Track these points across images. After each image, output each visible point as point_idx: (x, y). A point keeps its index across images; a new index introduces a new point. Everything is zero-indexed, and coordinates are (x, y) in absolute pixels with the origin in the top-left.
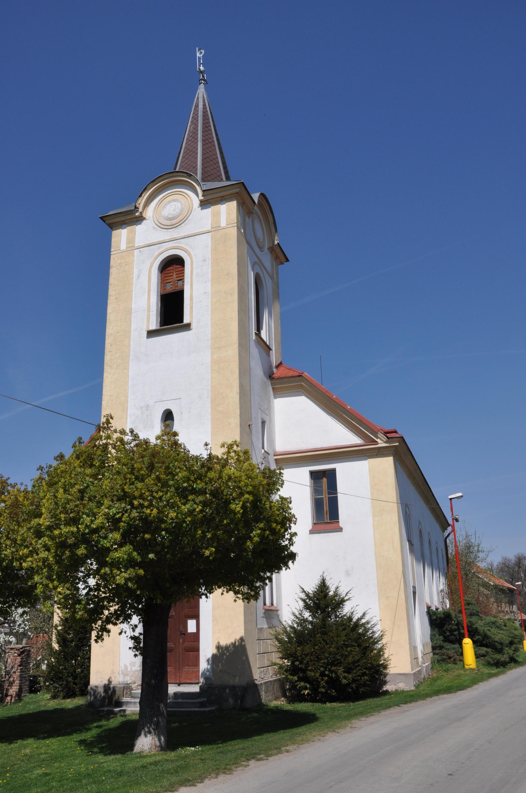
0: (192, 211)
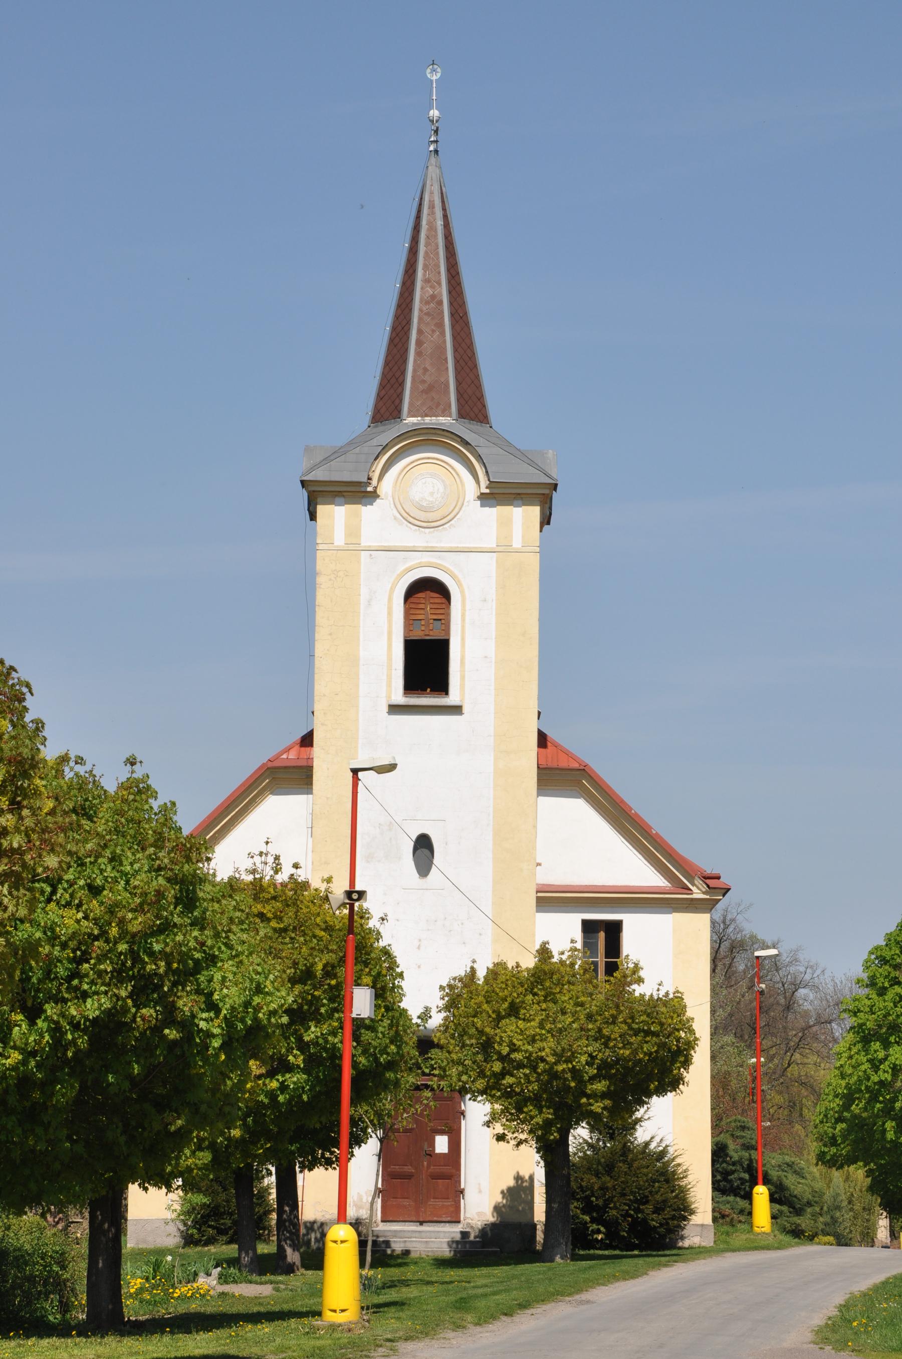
0: (463, 504)
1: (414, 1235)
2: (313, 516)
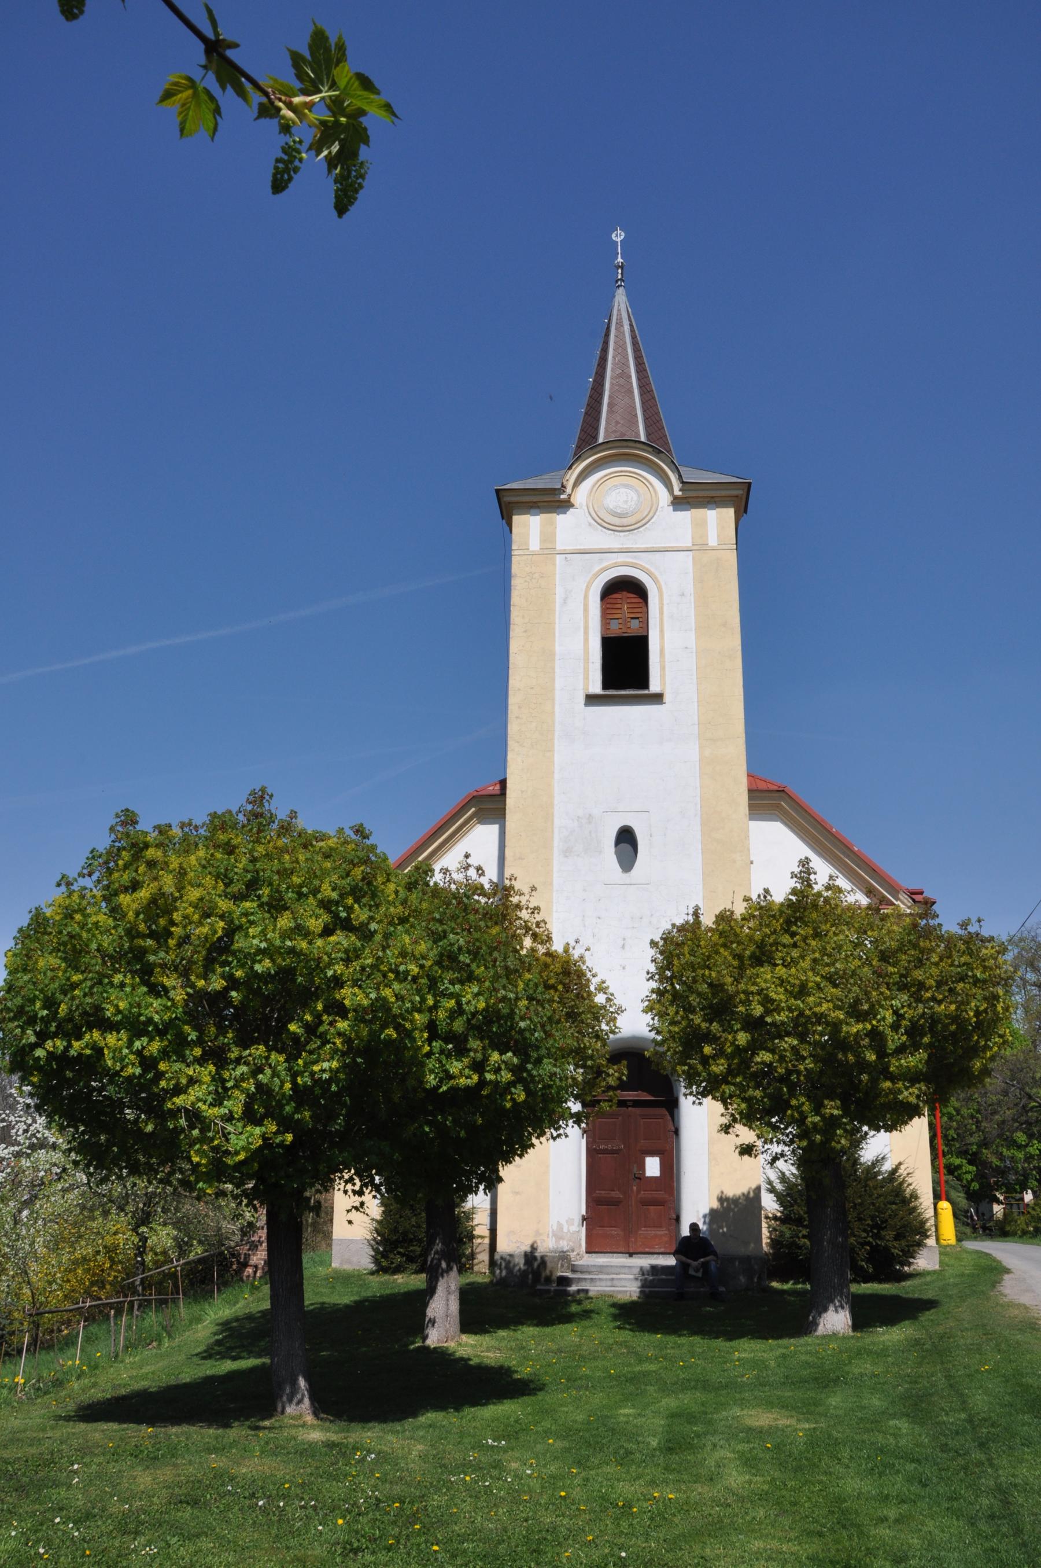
1: (623, 1271)
2: (510, 524)
